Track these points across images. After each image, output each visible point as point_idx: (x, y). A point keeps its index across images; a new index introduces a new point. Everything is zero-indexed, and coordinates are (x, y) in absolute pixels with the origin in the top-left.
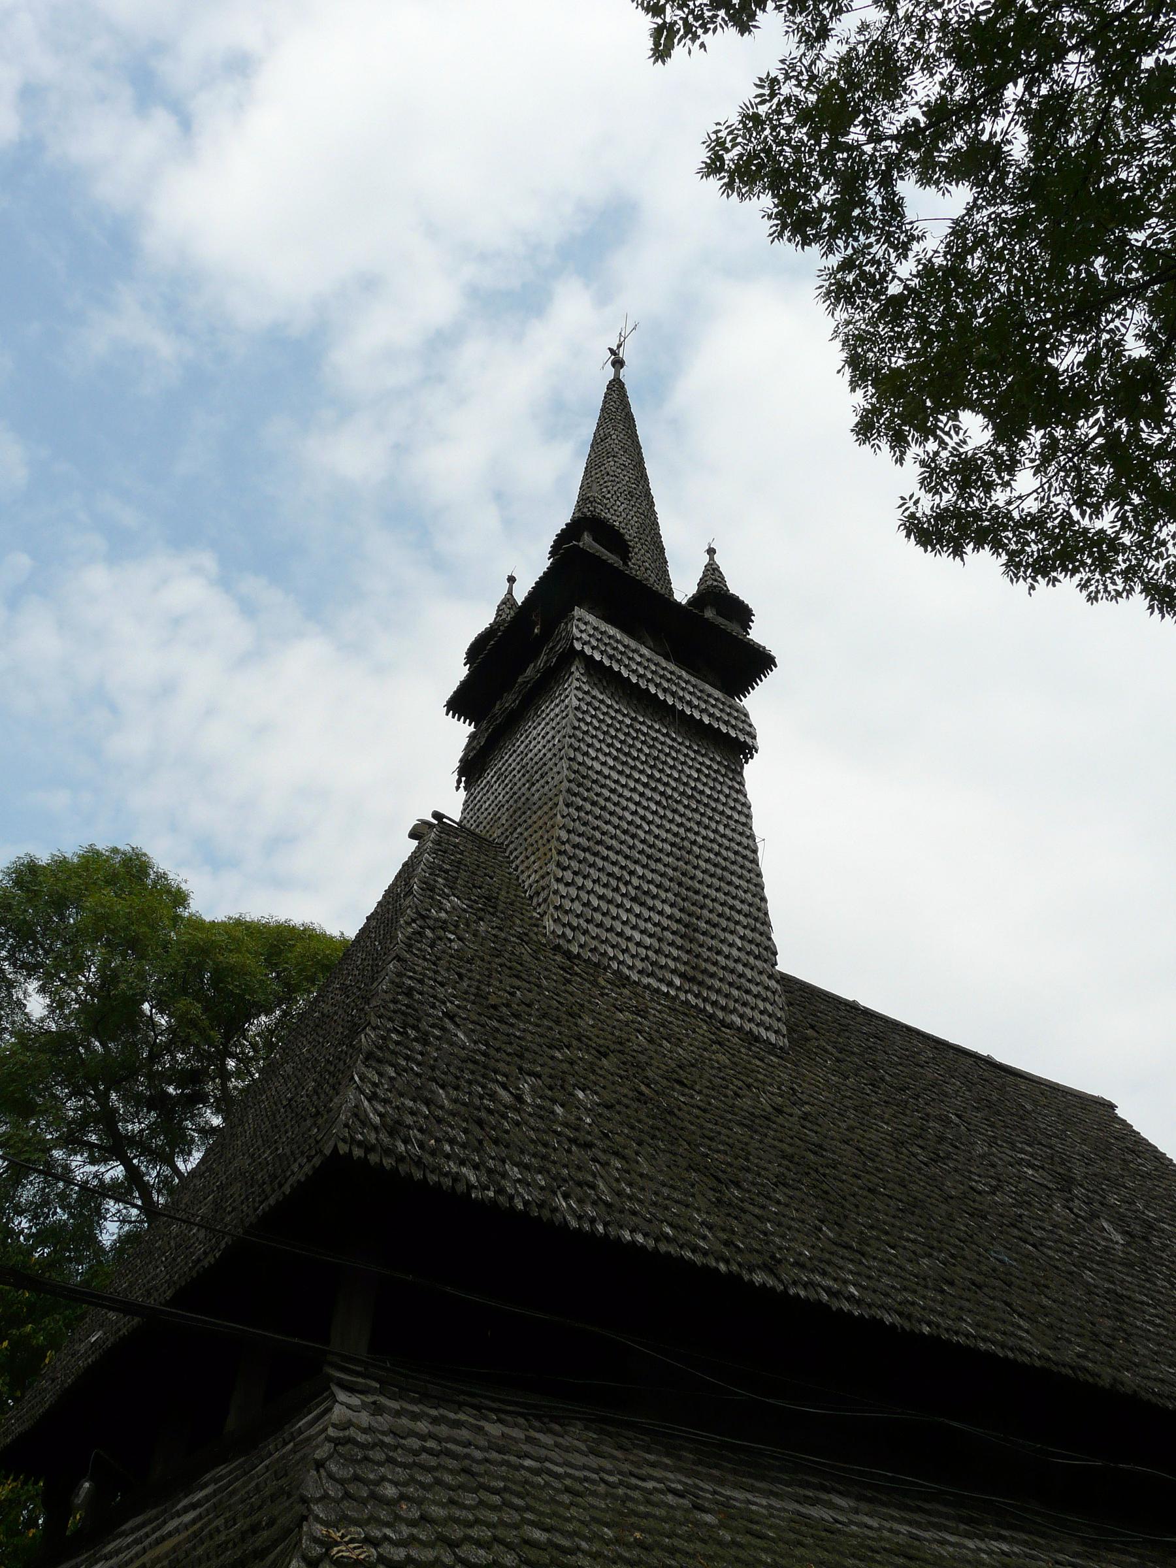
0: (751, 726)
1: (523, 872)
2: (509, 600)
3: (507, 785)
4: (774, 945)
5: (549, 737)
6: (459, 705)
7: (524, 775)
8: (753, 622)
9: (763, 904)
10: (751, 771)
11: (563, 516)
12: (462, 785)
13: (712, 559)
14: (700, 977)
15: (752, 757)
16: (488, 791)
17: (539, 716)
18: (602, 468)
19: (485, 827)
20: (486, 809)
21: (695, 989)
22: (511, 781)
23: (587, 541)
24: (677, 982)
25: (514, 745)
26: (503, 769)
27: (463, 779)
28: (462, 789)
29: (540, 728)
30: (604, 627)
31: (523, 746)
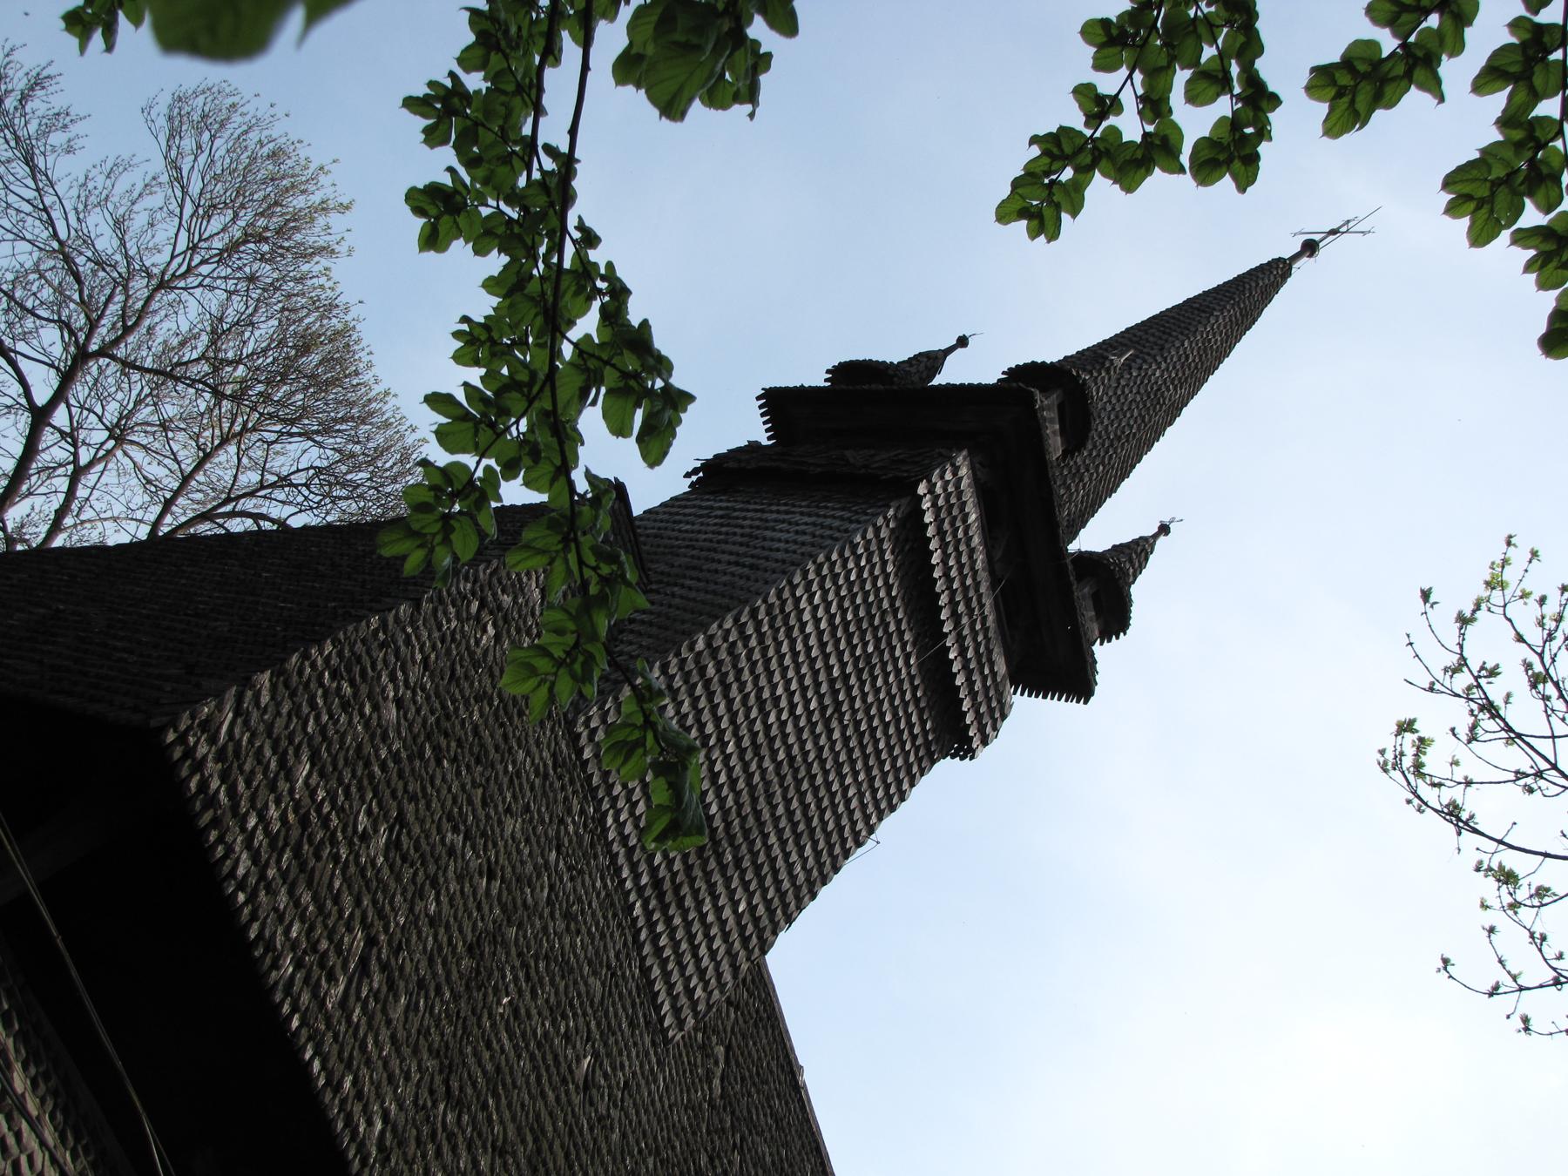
0: (995, 729)
1: (632, 631)
2: (933, 361)
3: (720, 533)
4: (772, 945)
5: (801, 538)
6: (777, 402)
7: (741, 544)
8: (1117, 638)
9: (806, 898)
10: (946, 768)
11: (1051, 353)
12: (694, 478)
13: (1156, 536)
14: (669, 897)
15: (962, 758)
16: (701, 516)
17: (818, 507)
18: (1165, 337)
19: (659, 546)
20: (680, 531)
21: (653, 903)
22: (727, 534)
23: (1047, 405)
24: (644, 880)
25: (771, 505)
26: (736, 514)
27: (701, 474)
28: (688, 481)
29: (806, 519)
30: (969, 497)
31: (774, 516)
